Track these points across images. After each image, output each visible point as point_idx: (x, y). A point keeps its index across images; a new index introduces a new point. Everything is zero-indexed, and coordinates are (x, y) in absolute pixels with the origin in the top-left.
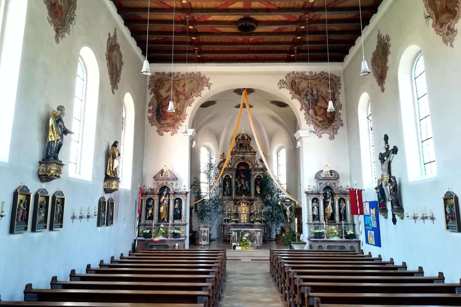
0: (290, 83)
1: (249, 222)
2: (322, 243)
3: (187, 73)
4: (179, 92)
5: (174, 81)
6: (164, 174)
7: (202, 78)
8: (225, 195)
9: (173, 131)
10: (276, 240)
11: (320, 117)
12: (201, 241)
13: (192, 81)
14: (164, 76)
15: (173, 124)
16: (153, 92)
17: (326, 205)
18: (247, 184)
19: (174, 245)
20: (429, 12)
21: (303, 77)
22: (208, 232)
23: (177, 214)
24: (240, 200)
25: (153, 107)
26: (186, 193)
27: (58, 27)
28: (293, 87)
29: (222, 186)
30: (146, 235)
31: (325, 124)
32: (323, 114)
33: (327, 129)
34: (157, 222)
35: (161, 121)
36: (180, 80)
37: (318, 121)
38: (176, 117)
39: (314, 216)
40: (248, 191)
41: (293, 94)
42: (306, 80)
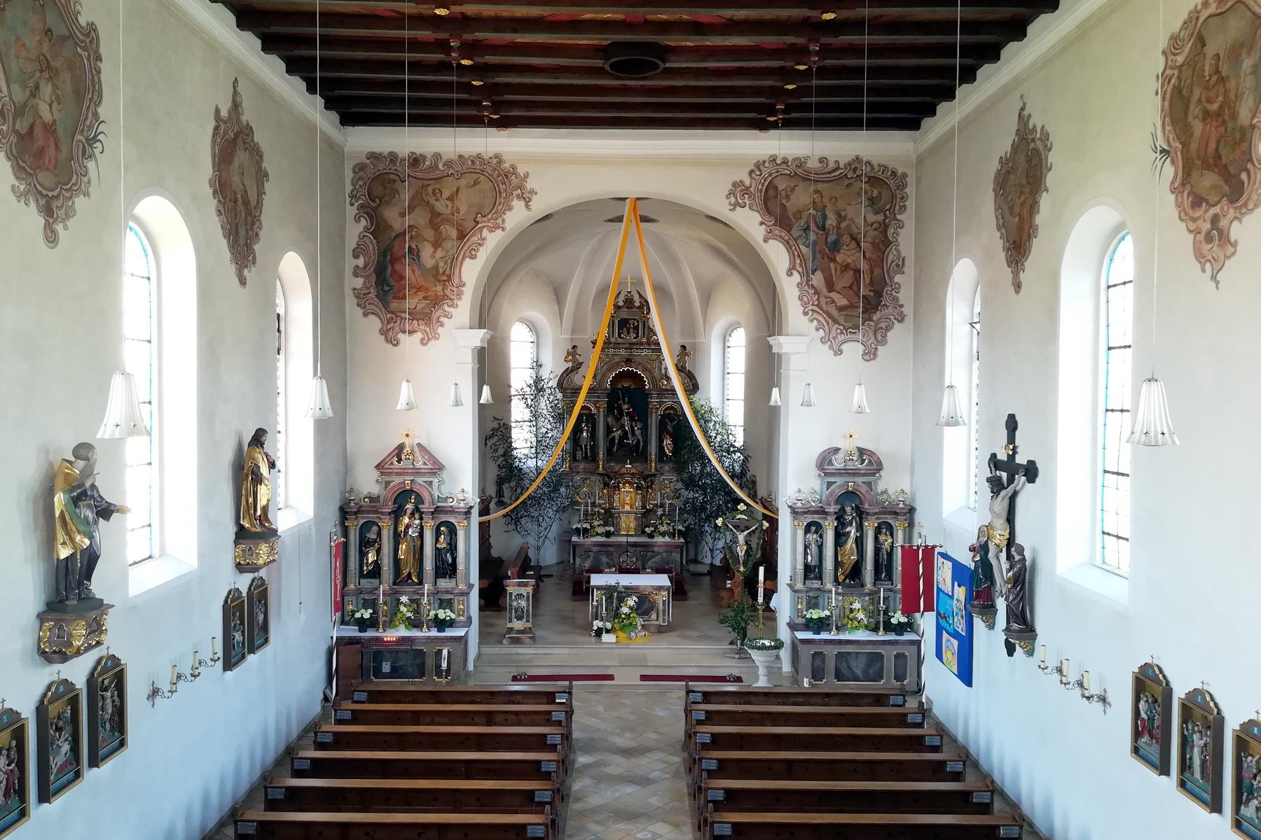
3: (461, 156)
4: (440, 214)
5: (424, 181)
8: (578, 459)
9: (425, 331)
11: (840, 293)
13: (476, 183)
14: (395, 165)
15: (426, 311)
16: (366, 216)
18: (640, 431)
19: (438, 650)
20: (1168, 137)
21: (799, 172)
23: (443, 564)
25: (367, 259)
27: (50, 194)
32: (850, 287)
35: (392, 302)
36: (442, 178)
37: (836, 306)
39: (808, 568)
40: (641, 448)
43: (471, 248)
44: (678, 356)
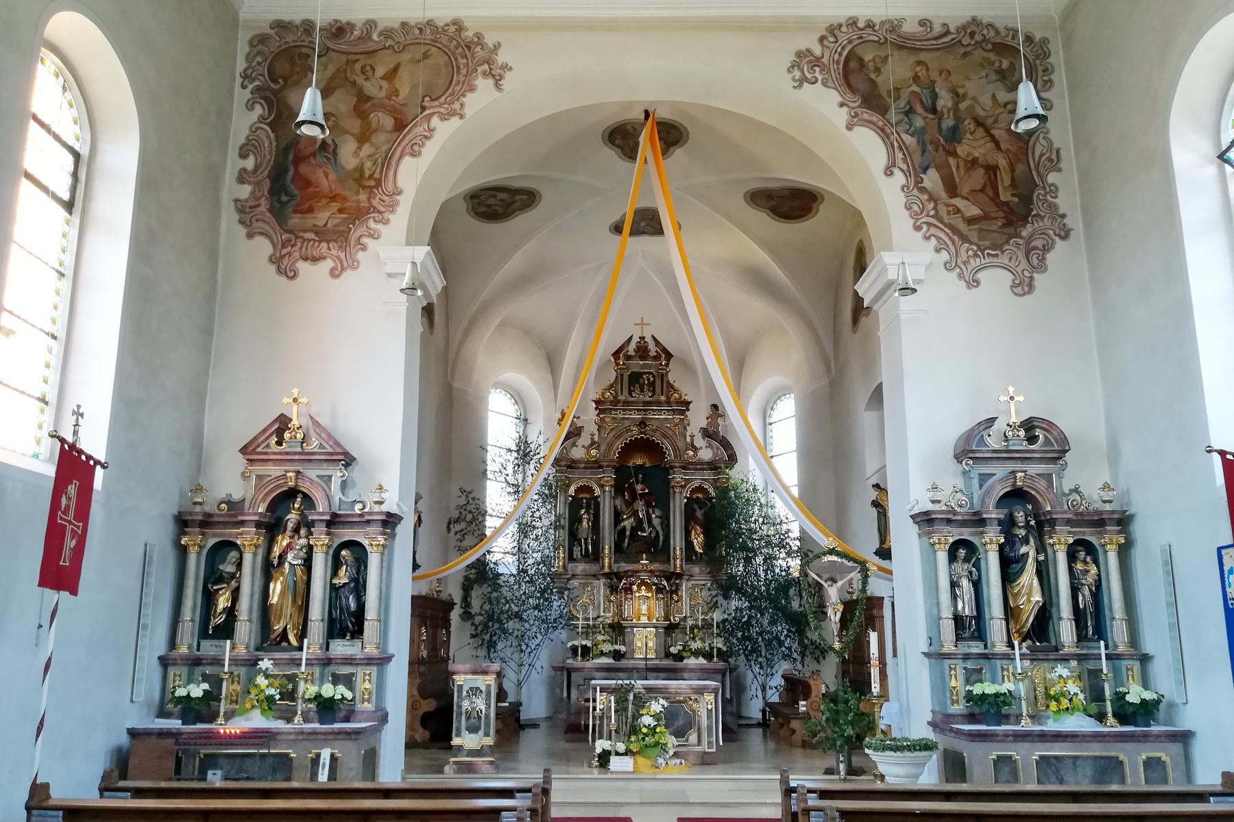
0: (838, 63)
2: (1013, 745)
3: (404, 24)
4: (369, 98)
6: (289, 435)
7: (469, 42)
9: (338, 257)
10: (764, 724)
12: (459, 735)
13: (426, 56)
15: (341, 228)
16: (263, 102)
17: (1010, 571)
22: (488, 694)
24: (630, 574)
26: (384, 517)
28: (852, 79)
29: (565, 522)
30: (195, 710)
31: (989, 228)
32: (982, 190)
33: (1003, 252)
34: (252, 649)
35: (292, 218)
36: (376, 51)
37: (963, 217)
38: (353, 201)
39: (958, 620)
40: (661, 543)
41: (853, 108)
42: (904, 52)
43: (413, 142)
44: (707, 418)
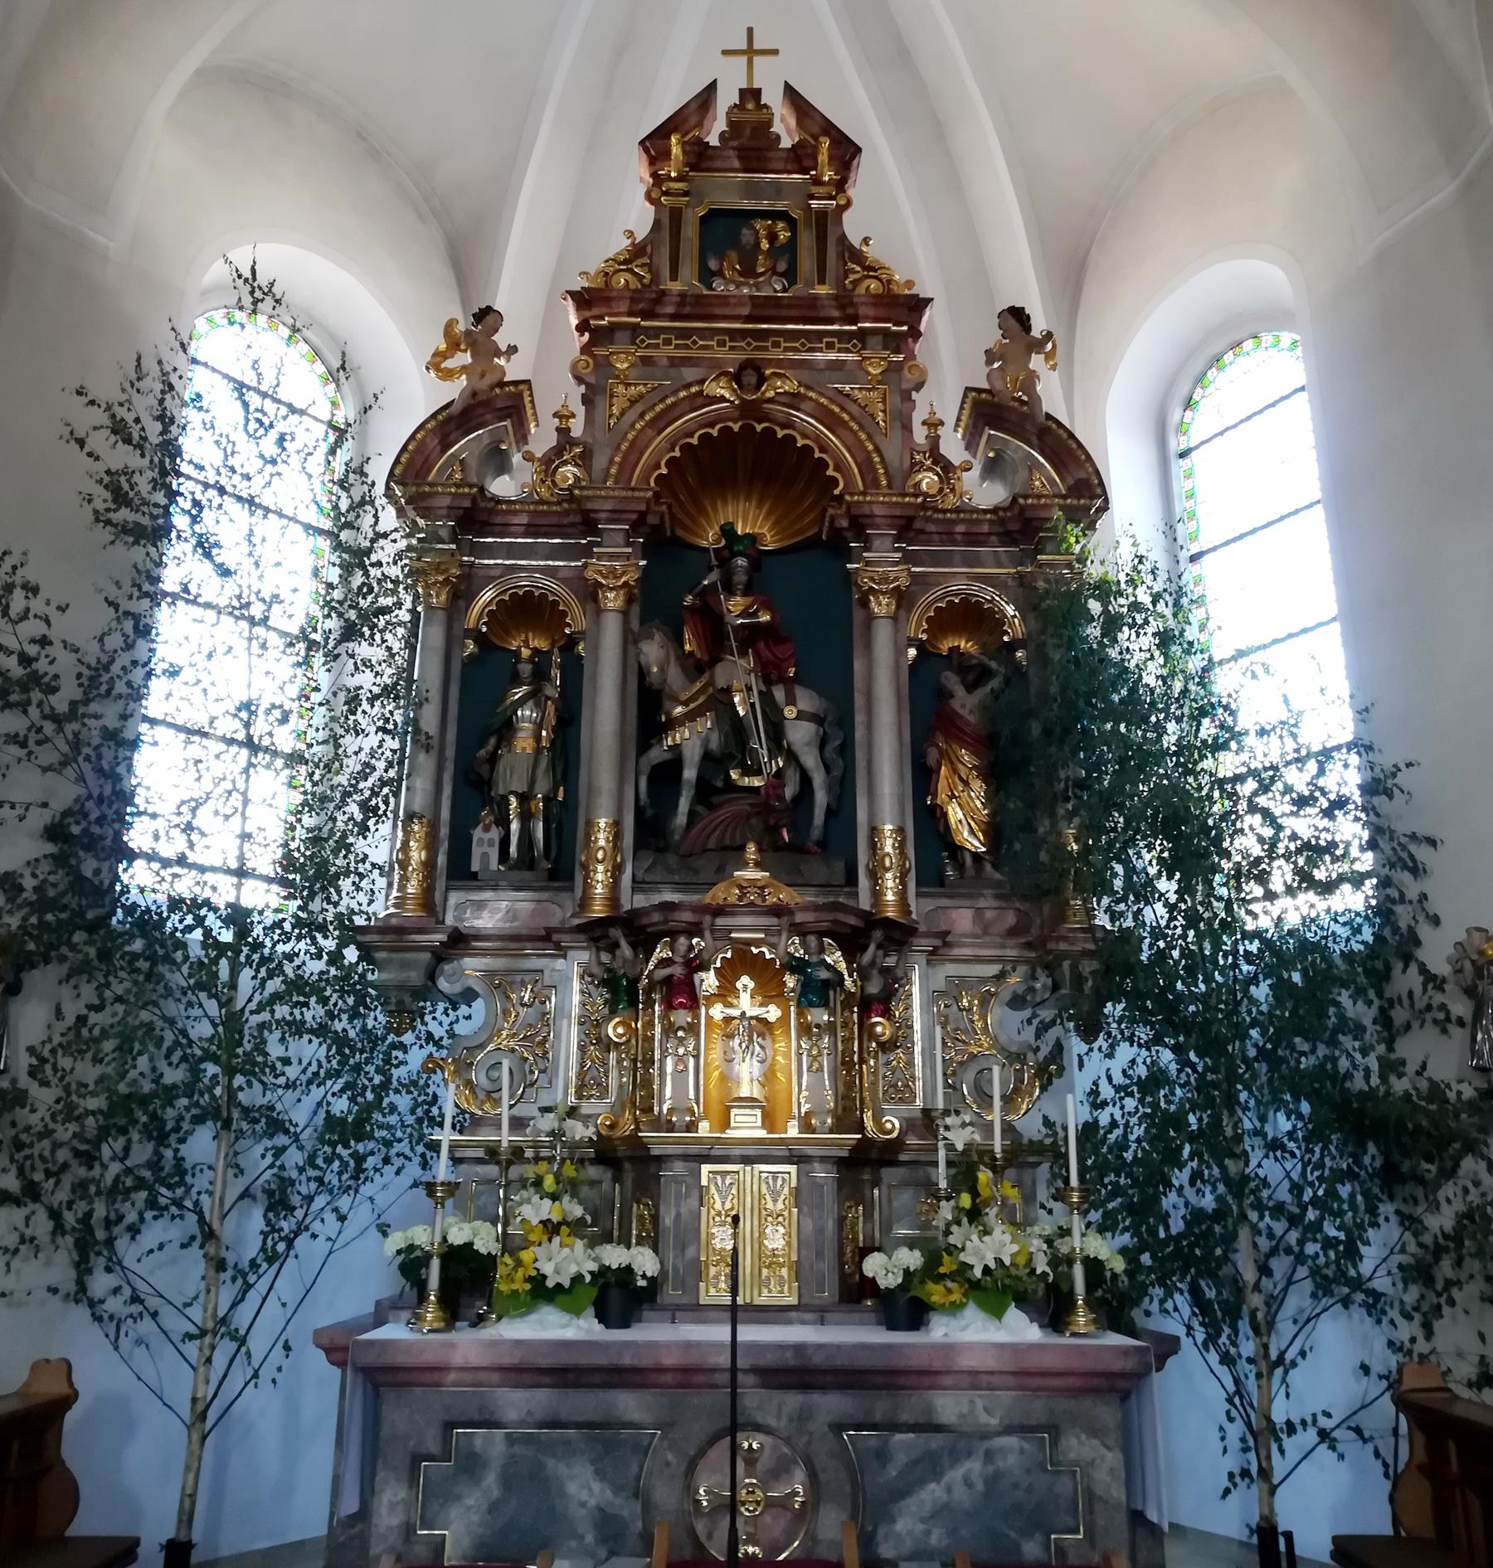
1: (828, 1294)
8: (475, 866)
